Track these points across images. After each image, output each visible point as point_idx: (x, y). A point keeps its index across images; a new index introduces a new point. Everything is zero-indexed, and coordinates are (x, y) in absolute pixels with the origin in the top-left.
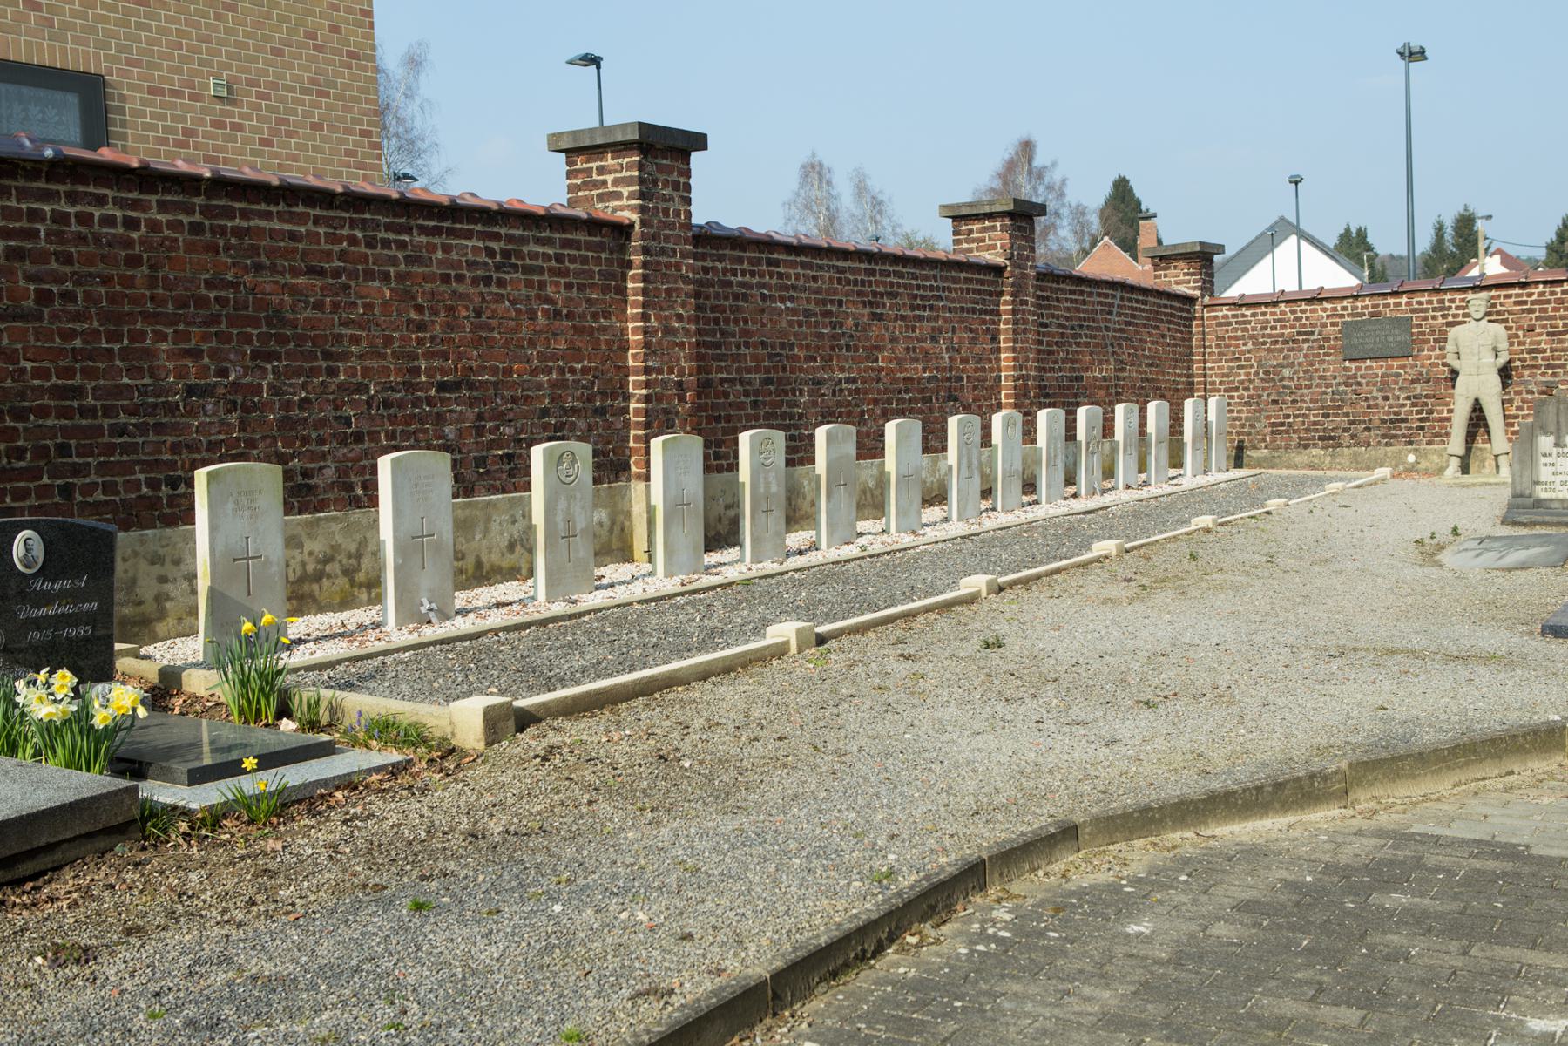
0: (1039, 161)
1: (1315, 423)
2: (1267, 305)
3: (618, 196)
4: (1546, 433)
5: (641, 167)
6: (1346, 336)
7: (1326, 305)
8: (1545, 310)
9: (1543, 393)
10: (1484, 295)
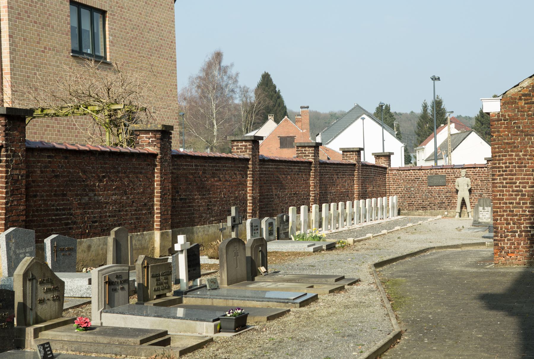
0: (223, 64)
1: (420, 203)
2: (407, 170)
3: (309, 156)
4: (481, 206)
5: (314, 150)
6: (429, 180)
7: (423, 171)
8: (480, 175)
9: (479, 196)
10: (465, 170)
